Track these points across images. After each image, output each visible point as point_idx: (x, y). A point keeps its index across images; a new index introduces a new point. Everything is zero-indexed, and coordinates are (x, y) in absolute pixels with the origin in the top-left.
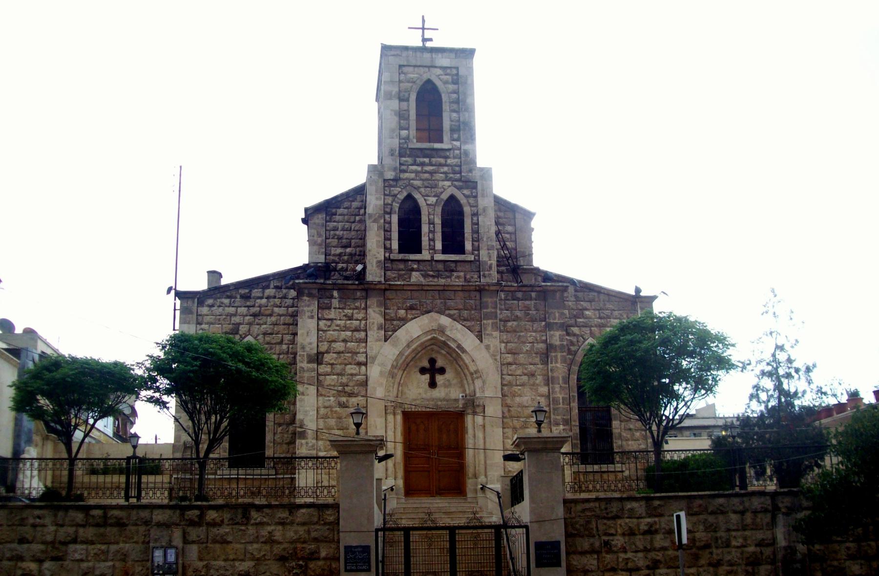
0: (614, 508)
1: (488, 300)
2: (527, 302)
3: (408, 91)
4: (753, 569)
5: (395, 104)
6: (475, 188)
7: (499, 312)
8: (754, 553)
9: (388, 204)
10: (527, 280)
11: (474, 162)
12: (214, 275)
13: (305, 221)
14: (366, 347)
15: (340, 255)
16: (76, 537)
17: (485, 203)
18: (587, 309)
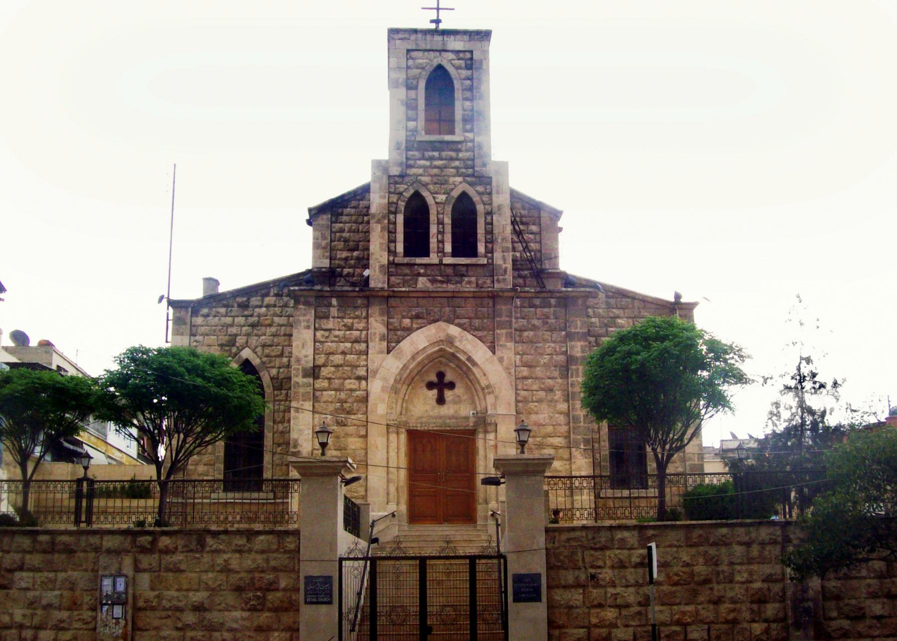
0: (603, 537)
1: (503, 308)
2: (546, 310)
3: (417, 78)
4: (759, 609)
5: (402, 92)
6: (490, 183)
7: (514, 320)
8: (760, 589)
9: (393, 203)
10: (551, 285)
11: (488, 155)
12: (211, 282)
13: (309, 222)
14: (367, 360)
15: (346, 259)
16: (23, 564)
17: (501, 200)
18: (619, 317)
